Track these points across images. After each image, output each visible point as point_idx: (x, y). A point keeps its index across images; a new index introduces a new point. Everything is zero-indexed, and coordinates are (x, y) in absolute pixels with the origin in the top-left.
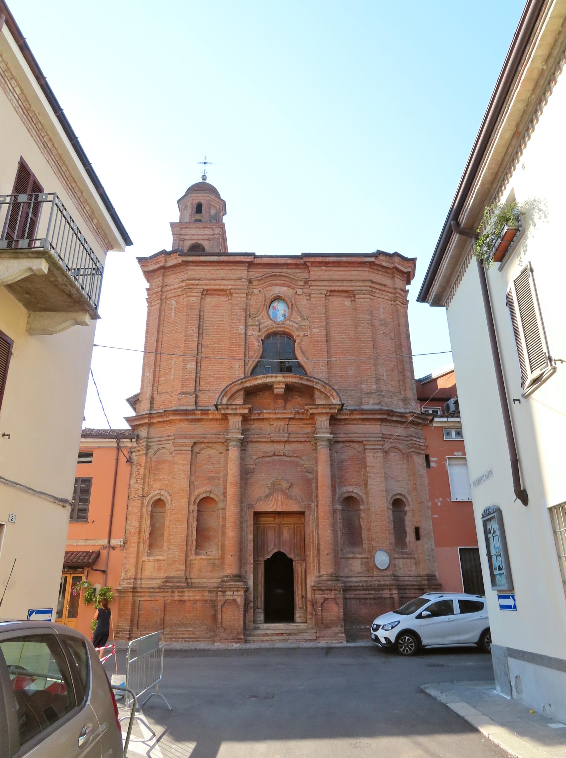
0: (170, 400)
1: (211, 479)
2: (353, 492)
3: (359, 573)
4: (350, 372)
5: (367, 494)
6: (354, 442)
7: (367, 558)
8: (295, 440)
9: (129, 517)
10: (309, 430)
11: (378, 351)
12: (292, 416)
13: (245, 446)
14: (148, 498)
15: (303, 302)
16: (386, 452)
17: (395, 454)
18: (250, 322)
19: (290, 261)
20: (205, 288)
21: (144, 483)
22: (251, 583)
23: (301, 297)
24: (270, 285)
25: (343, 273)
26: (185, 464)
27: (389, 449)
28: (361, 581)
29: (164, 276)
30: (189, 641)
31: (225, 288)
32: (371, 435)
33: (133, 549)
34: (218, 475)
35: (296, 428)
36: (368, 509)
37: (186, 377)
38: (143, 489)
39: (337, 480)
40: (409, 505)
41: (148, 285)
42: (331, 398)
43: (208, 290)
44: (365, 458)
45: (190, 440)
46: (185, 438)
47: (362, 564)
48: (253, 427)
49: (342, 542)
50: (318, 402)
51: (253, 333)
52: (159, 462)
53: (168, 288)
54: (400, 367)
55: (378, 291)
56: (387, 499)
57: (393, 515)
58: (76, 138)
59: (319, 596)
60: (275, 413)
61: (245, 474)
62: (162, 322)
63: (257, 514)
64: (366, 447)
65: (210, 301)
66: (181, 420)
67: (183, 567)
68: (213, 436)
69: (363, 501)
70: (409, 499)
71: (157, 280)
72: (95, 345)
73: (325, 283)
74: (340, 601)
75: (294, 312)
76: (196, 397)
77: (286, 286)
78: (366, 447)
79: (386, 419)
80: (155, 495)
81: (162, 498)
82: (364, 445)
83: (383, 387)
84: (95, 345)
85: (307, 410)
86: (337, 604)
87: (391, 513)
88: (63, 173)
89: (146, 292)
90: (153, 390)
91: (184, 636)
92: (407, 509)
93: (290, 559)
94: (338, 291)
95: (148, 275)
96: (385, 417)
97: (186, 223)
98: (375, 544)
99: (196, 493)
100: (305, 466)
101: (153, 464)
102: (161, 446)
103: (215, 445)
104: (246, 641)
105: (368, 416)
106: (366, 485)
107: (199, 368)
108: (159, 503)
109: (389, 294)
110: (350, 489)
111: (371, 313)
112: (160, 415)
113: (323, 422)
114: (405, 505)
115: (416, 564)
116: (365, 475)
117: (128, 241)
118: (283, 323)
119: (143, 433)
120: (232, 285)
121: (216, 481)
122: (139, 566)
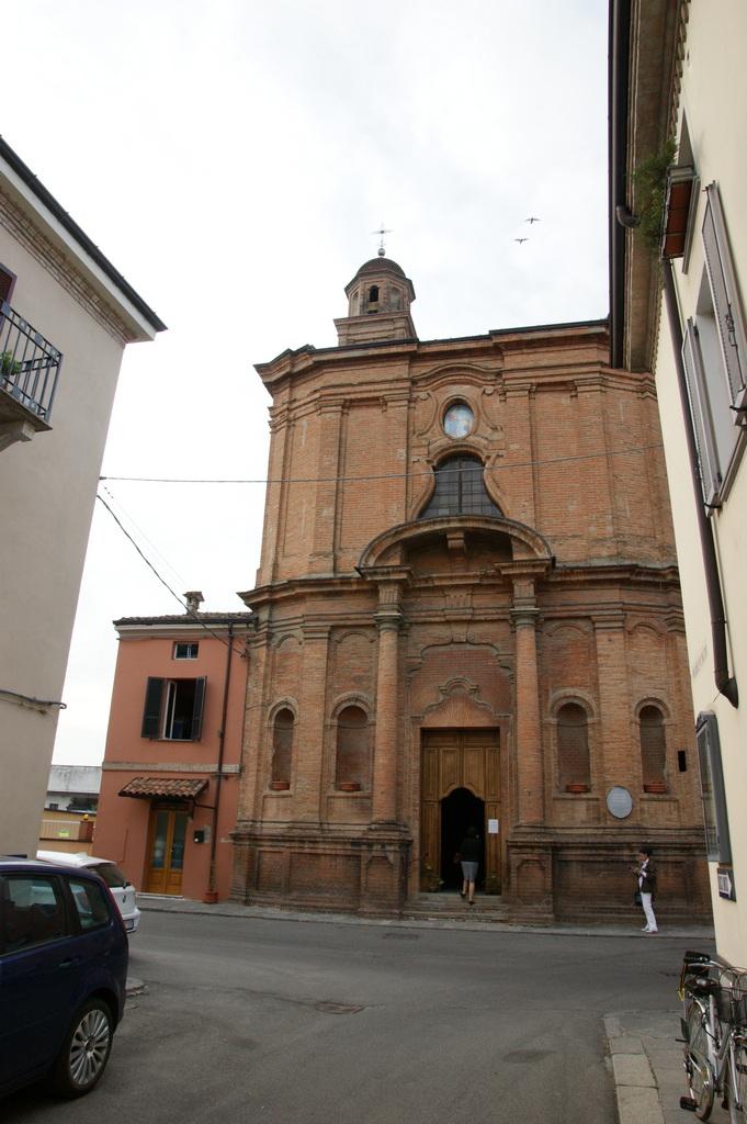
0: (299, 566)
1: (357, 680)
2: (575, 697)
3: (583, 822)
4: (571, 508)
5: (597, 699)
6: (577, 618)
7: (597, 799)
8: (482, 618)
9: (247, 734)
10: (503, 601)
11: (616, 472)
12: (477, 581)
13: (408, 629)
14: (270, 708)
15: (495, 403)
16: (630, 633)
17: (645, 635)
18: (414, 440)
19: (472, 345)
20: (347, 397)
21: (264, 687)
22: (415, 834)
23: (491, 398)
24: (443, 385)
25: (558, 354)
26: (319, 659)
27: (635, 627)
28: (586, 835)
29: (292, 387)
30: (324, 912)
31: (376, 394)
32: (605, 606)
33: (251, 777)
34: (368, 674)
35: (488, 603)
36: (600, 723)
37: (320, 530)
38: (264, 695)
39: (550, 679)
40: (669, 715)
41: (270, 401)
42: (536, 550)
43: (352, 401)
44: (595, 642)
45: (325, 623)
46: (319, 620)
47: (588, 810)
48: (419, 600)
49: (557, 775)
50: (517, 557)
51: (419, 455)
52: (286, 656)
53: (297, 404)
54: (654, 496)
55: (614, 379)
56: (630, 707)
57: (641, 732)
58: (34, 177)
59: (515, 858)
60: (451, 578)
61: (408, 674)
62: (289, 453)
63: (428, 734)
64: (597, 625)
65: (357, 415)
66: (312, 594)
67: (316, 808)
68: (359, 616)
69: (591, 710)
70: (669, 706)
71: (283, 393)
72: (101, 478)
73: (529, 374)
74: (548, 865)
75: (482, 423)
76: (335, 560)
77: (467, 384)
78: (597, 625)
79: (628, 579)
80: (280, 704)
81: (289, 708)
82: (594, 623)
83: (627, 530)
84: (101, 478)
85: (499, 571)
86: (543, 869)
87: (636, 730)
88: (25, 232)
89: (268, 412)
90: (277, 553)
91: (316, 904)
92: (665, 721)
93: (479, 800)
94: (550, 384)
95: (272, 387)
96: (627, 576)
97: (356, 317)
98: (609, 778)
99: (336, 700)
100: (500, 658)
101: (277, 659)
102: (288, 633)
103: (362, 630)
104: (401, 917)
105: (596, 577)
106: (596, 685)
107: (339, 516)
108: (285, 716)
109: (633, 382)
110: (570, 691)
111: (604, 412)
112: (284, 587)
113: (524, 589)
114: (663, 717)
115: (678, 809)
116: (597, 671)
117: (158, 326)
118: (464, 439)
119: (264, 615)
120: (387, 390)
121: (365, 683)
122: (260, 805)
